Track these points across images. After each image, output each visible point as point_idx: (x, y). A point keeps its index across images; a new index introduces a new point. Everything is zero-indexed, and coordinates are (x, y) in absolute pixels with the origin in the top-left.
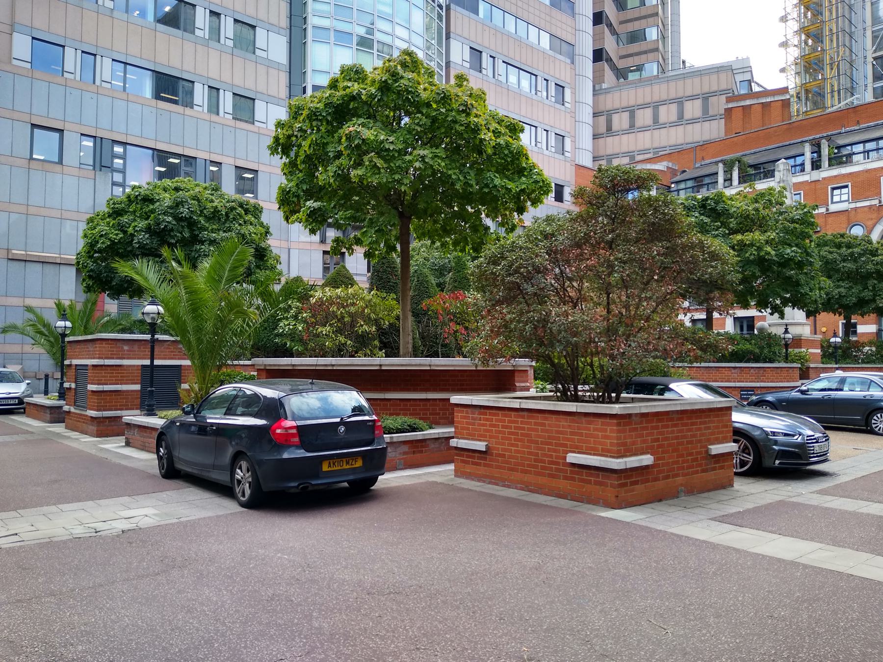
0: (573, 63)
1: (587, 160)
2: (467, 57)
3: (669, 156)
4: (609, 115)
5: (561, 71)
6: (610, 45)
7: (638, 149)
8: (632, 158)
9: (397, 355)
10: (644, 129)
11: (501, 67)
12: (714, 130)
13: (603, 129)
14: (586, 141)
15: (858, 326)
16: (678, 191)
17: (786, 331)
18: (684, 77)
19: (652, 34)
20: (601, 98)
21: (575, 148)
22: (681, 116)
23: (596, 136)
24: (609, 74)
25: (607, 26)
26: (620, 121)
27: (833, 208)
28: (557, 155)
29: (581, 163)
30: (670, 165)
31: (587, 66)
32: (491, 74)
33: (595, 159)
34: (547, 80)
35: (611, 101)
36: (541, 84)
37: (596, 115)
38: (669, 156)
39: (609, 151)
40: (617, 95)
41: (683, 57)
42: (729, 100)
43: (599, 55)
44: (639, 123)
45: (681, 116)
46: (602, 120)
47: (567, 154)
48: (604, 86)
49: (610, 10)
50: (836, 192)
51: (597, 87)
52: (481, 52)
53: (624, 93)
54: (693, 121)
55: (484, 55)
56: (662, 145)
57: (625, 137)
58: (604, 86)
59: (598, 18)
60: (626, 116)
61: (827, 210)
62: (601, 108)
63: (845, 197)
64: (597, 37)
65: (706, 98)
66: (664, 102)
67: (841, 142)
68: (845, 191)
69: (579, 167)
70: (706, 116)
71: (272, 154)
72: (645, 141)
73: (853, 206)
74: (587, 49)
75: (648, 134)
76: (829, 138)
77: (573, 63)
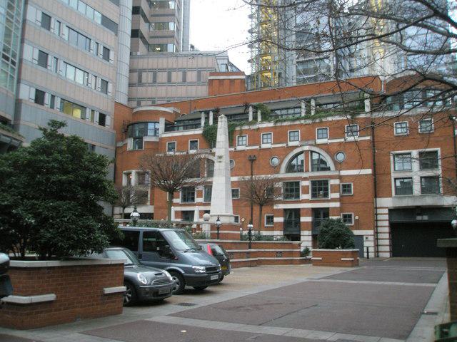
0: (116, 35)
1: (123, 100)
2: (40, 18)
3: (175, 104)
4: (140, 72)
5: (107, 38)
6: (144, 28)
7: (178, 96)
8: (154, 102)
9: (313, 209)
10: (162, 84)
11: (65, 31)
12: (202, 92)
13: (135, 80)
14: (124, 88)
15: (275, 218)
16: (178, 126)
17: (218, 220)
18: (193, 56)
19: (172, 26)
20: (136, 61)
21: (116, 91)
22: (184, 80)
23: (131, 85)
24: (142, 49)
25: (142, 16)
26: (147, 77)
27: (263, 146)
28: (102, 94)
29: (119, 101)
30: (176, 110)
31: (126, 39)
32: (57, 33)
33: (130, 100)
34: (98, 44)
35: (142, 64)
36: (93, 46)
37: (131, 71)
38: (175, 104)
39: (139, 96)
40: (146, 60)
41: (191, 42)
42: (212, 74)
43: (135, 33)
44: (159, 80)
45: (184, 80)
46: (136, 75)
47: (109, 94)
48: (138, 53)
49: (145, 7)
50: (265, 137)
51: (134, 54)
52: (50, 17)
53: (160, 60)
54: (192, 84)
55: (53, 20)
56: (173, 96)
57: (150, 88)
58: (138, 53)
59: (136, 10)
60: (180, 74)
61: (187, 153)
62: (135, 67)
63: (244, 143)
64: (133, 22)
65: (199, 71)
66: (175, 70)
67: (321, 102)
68: (269, 136)
69: (117, 104)
70: (199, 82)
71: (249, 31)
72: (162, 92)
73: (330, 141)
74: (127, 28)
75: (164, 88)
76: (315, 99)
77: (116, 35)
